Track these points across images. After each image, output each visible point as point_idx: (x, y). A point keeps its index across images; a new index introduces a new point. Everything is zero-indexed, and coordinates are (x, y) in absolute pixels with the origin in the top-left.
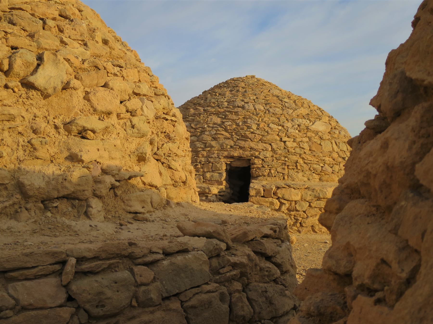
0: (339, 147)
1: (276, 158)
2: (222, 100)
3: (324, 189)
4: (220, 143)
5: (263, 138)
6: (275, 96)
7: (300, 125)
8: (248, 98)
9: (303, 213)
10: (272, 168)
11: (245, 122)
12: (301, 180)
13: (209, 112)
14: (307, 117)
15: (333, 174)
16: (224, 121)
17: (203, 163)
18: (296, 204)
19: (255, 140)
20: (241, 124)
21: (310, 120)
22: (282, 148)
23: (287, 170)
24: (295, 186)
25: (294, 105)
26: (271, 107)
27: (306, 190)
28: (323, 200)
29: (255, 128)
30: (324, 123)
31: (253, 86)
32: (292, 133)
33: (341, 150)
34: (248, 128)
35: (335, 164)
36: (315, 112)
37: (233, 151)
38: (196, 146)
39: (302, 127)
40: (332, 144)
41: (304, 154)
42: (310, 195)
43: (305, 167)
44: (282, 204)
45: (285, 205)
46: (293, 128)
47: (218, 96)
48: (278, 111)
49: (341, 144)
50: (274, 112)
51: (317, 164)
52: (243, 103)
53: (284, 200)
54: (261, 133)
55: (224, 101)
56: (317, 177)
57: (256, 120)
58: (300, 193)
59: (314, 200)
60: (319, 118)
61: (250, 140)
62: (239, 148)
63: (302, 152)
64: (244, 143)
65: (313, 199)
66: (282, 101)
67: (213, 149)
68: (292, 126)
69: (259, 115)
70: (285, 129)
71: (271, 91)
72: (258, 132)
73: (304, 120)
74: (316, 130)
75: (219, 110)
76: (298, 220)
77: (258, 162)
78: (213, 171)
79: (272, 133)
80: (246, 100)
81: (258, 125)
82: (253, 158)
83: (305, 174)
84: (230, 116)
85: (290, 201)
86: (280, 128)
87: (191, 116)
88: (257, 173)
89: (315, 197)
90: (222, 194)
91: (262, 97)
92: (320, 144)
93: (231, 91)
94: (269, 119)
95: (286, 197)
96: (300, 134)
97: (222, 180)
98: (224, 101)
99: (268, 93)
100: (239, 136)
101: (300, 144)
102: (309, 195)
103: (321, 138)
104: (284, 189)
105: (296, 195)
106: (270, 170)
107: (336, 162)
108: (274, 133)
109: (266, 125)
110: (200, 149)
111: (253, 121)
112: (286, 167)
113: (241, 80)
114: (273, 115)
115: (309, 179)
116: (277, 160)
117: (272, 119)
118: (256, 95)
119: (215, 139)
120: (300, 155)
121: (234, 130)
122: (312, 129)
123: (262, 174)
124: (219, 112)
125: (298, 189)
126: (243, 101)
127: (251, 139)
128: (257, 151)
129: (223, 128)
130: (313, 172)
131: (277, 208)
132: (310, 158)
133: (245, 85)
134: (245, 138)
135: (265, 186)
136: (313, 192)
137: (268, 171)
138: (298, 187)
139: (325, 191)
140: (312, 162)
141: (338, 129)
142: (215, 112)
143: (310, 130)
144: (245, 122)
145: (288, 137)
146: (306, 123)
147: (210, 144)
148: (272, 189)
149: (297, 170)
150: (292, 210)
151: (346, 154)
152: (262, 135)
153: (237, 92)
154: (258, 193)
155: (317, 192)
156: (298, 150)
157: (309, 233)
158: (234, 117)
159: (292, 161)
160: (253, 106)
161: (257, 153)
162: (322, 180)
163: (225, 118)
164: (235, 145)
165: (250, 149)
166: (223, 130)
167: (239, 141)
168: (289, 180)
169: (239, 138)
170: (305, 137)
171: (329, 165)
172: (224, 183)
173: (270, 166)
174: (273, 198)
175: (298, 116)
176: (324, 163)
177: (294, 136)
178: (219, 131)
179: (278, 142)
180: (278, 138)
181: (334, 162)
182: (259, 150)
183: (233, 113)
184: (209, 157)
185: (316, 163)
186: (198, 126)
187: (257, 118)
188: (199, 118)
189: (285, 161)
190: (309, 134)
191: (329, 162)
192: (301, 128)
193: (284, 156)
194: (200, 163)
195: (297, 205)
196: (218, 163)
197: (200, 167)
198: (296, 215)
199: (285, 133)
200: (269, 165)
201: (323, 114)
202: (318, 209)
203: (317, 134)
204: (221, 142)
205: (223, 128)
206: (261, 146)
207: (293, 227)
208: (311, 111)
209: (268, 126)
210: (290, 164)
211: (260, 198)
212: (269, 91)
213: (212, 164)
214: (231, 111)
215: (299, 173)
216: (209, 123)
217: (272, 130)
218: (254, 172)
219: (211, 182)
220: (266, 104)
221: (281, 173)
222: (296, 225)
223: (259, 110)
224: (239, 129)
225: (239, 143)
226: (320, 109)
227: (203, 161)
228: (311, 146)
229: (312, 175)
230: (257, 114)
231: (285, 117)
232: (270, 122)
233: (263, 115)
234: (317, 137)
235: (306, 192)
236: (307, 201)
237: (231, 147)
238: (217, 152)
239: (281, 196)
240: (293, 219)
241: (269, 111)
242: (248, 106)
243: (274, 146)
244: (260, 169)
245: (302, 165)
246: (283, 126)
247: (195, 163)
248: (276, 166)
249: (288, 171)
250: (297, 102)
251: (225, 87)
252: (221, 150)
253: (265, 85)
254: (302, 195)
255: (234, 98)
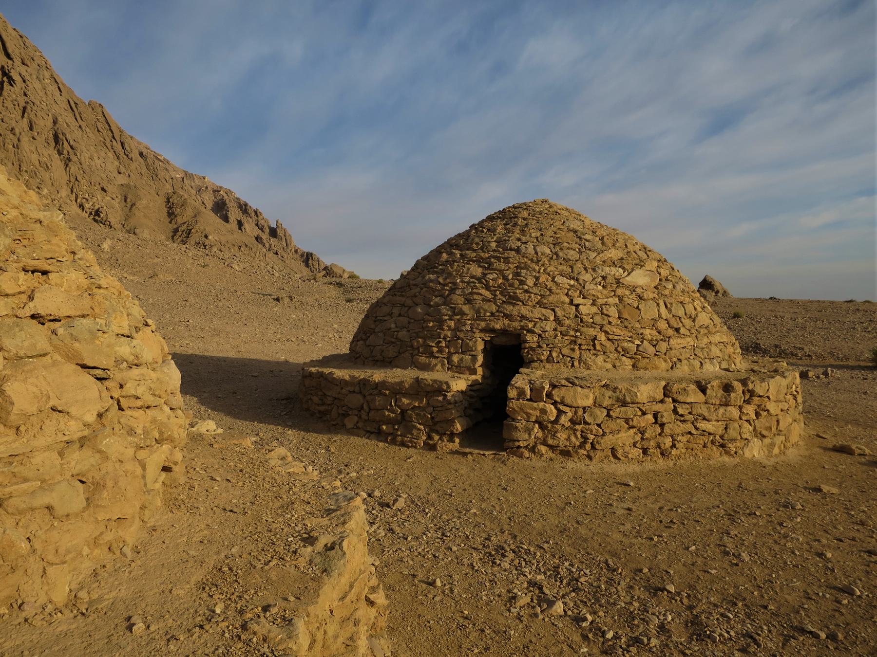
0: (670, 311)
1: (561, 332)
2: (489, 239)
3: (634, 387)
4: (476, 309)
5: (543, 299)
6: (571, 231)
7: (606, 277)
8: (528, 235)
9: (596, 427)
10: (554, 348)
11: (517, 274)
12: (601, 368)
13: (467, 258)
14: (619, 263)
15: (656, 358)
16: (486, 272)
17: (448, 339)
18: (584, 412)
19: (530, 303)
20: (510, 277)
21: (623, 268)
22: (571, 316)
23: (578, 352)
24: (583, 383)
25: (599, 245)
26: (561, 249)
27: (603, 389)
28: (630, 405)
29: (531, 284)
30: (649, 272)
31: (540, 216)
32: (590, 292)
33: (673, 316)
34: (520, 284)
35: (662, 340)
36: (634, 254)
37: (494, 322)
38: (440, 312)
39: (610, 279)
40: (659, 307)
41: (609, 326)
42: (610, 398)
43: (608, 346)
44: (560, 412)
45: (566, 415)
46: (594, 282)
47: (486, 234)
48: (572, 256)
49: (674, 305)
50: (565, 257)
51: (629, 341)
52: (519, 243)
53: (565, 405)
54: (540, 291)
55: (493, 240)
56: (628, 362)
57: (534, 270)
58: (591, 395)
59: (617, 406)
60: (641, 264)
61: (521, 303)
62: (503, 317)
63: (605, 323)
64: (511, 307)
65: (614, 405)
66: (580, 238)
67: (465, 317)
68: (592, 279)
69: (541, 263)
70: (580, 284)
71: (567, 224)
72: (535, 290)
73: (613, 269)
74: (632, 284)
75: (482, 254)
76: (588, 439)
77: (531, 340)
78: (463, 353)
79: (558, 291)
80: (524, 239)
81: (537, 278)
82: (525, 332)
83: (609, 357)
84: (496, 265)
85: (574, 407)
86: (572, 282)
87: (441, 265)
88: (530, 356)
89: (617, 401)
90: (474, 388)
91: (550, 233)
92: (638, 308)
93: (506, 224)
94: (557, 268)
95: (568, 401)
96: (605, 292)
97: (477, 366)
98: (493, 240)
99: (562, 227)
100: (505, 296)
101: (602, 309)
102: (608, 398)
103: (640, 298)
104: (564, 389)
105: (584, 397)
106: (550, 351)
107: (663, 336)
108: (560, 291)
109: (550, 278)
110: (446, 318)
111: (530, 272)
112: (577, 347)
113: (525, 207)
114: (563, 262)
115: (614, 367)
116: (563, 335)
117: (560, 268)
118: (541, 230)
119: (469, 301)
120: (602, 326)
121: (499, 287)
122: (626, 283)
123: (537, 358)
124: (482, 258)
125: (589, 387)
126: (519, 239)
127: (522, 302)
128: (530, 321)
129: (483, 283)
130: (622, 354)
131: (552, 419)
132: (618, 331)
133: (529, 215)
134: (514, 300)
135: (532, 382)
136: (615, 392)
137: (546, 353)
138: (589, 385)
139: (635, 391)
140: (622, 338)
141: (671, 281)
142: (475, 259)
143: (623, 284)
144: (517, 274)
145: (584, 298)
146: (617, 274)
147: (461, 309)
148: (544, 388)
149: (594, 352)
150: (578, 421)
151: (682, 322)
152: (541, 295)
153: (514, 226)
154: (521, 393)
155: (621, 392)
156: (598, 319)
157: (606, 461)
158: (503, 266)
159: (587, 336)
160: (534, 248)
161: (530, 325)
162: (637, 367)
163: (488, 268)
164: (497, 311)
165: (521, 317)
166: (483, 288)
167: (505, 306)
168: (582, 367)
169: (505, 300)
170: (612, 297)
171: (650, 341)
172: (480, 371)
173: (551, 346)
174: (545, 402)
175: (604, 262)
176: (642, 338)
177: (593, 295)
178: (476, 289)
179: (566, 306)
180: (567, 300)
181: (659, 337)
182: (534, 319)
183: (502, 260)
184: (458, 331)
185: (628, 339)
186: (448, 280)
187: (537, 268)
188: (452, 268)
189: (576, 337)
190: (619, 292)
191: (650, 337)
192: (607, 281)
193: (574, 329)
194: (444, 338)
195: (586, 414)
196: (470, 340)
197: (444, 345)
198: (585, 431)
199: (578, 291)
200: (549, 344)
201: (648, 256)
202: (624, 420)
203: (634, 291)
204: (477, 306)
205: (483, 283)
206: (538, 312)
207: (579, 451)
208: (628, 252)
209: (553, 280)
210: (584, 342)
211: (525, 402)
212: (564, 222)
213: (463, 340)
214: (499, 257)
215: (598, 357)
216: (465, 276)
217: (559, 286)
218: (525, 354)
219: (460, 370)
220: (554, 245)
221: (568, 356)
222: (585, 447)
223: (542, 255)
224: (507, 285)
225: (504, 308)
226: (645, 248)
227: (450, 336)
228: (622, 311)
229: (620, 360)
230: (538, 261)
231: (582, 264)
232: (556, 273)
233: (546, 262)
234: (633, 296)
235: (602, 393)
236: (605, 408)
237: (492, 314)
238: (470, 322)
239: (558, 400)
240: (579, 436)
241: (557, 256)
242: (526, 247)
243: (560, 313)
244: (534, 350)
245: (604, 343)
246: (577, 280)
247: (438, 340)
248: (559, 345)
249: (581, 354)
250: (605, 239)
251: (500, 218)
252: (476, 320)
253: (559, 214)
254: (596, 398)
255: (506, 236)
